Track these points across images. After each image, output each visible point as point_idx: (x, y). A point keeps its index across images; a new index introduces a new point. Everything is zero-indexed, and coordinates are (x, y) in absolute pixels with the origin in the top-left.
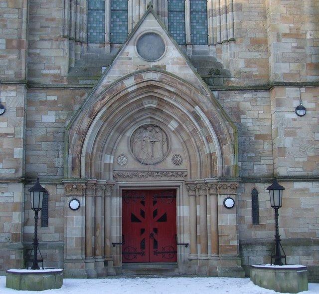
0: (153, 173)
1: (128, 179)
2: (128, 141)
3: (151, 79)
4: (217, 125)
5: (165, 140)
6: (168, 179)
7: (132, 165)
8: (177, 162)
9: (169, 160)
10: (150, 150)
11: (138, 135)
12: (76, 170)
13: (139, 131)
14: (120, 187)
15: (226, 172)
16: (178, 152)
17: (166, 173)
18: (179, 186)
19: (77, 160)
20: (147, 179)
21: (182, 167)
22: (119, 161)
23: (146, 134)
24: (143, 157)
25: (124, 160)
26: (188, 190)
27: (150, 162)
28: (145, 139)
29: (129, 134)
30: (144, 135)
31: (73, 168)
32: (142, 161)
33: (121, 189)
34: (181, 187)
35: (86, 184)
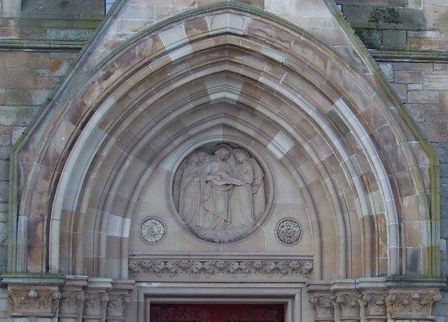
0: (227, 263)
1: (165, 277)
2: (167, 188)
3: (228, 30)
4: (388, 147)
5: (259, 181)
6: (264, 277)
7: (176, 243)
8: (288, 238)
9: (269, 230)
10: (221, 207)
11: (192, 169)
12: (38, 253)
13: (195, 159)
14: (146, 296)
15: (409, 263)
16: (290, 213)
17: (262, 265)
18: (293, 297)
19: (40, 230)
20: (213, 278)
21: (306, 246)
22: (145, 232)
23: (214, 166)
24: (204, 223)
25: (158, 228)
26: (315, 306)
27: (221, 235)
28: (210, 178)
29: (170, 165)
30: (208, 169)
31: (30, 248)
32: (202, 233)
33: (149, 301)
34: (297, 298)
35: (61, 288)
